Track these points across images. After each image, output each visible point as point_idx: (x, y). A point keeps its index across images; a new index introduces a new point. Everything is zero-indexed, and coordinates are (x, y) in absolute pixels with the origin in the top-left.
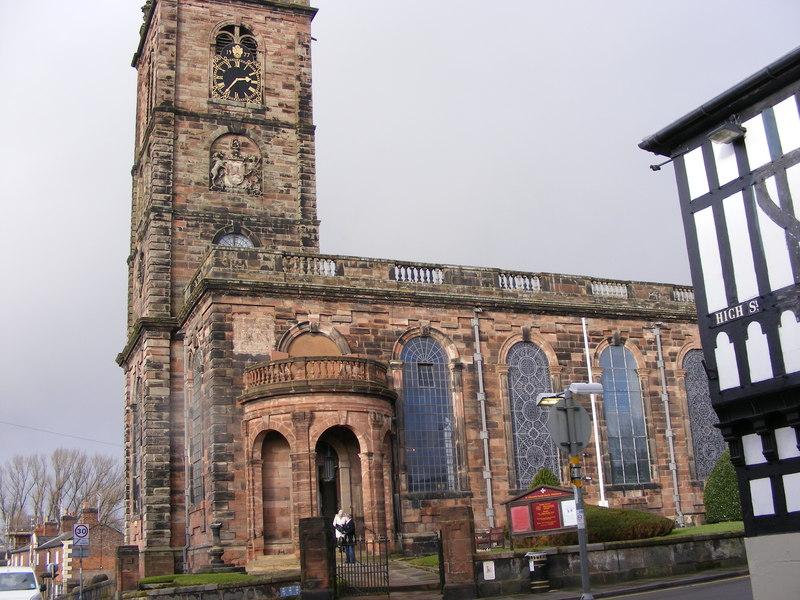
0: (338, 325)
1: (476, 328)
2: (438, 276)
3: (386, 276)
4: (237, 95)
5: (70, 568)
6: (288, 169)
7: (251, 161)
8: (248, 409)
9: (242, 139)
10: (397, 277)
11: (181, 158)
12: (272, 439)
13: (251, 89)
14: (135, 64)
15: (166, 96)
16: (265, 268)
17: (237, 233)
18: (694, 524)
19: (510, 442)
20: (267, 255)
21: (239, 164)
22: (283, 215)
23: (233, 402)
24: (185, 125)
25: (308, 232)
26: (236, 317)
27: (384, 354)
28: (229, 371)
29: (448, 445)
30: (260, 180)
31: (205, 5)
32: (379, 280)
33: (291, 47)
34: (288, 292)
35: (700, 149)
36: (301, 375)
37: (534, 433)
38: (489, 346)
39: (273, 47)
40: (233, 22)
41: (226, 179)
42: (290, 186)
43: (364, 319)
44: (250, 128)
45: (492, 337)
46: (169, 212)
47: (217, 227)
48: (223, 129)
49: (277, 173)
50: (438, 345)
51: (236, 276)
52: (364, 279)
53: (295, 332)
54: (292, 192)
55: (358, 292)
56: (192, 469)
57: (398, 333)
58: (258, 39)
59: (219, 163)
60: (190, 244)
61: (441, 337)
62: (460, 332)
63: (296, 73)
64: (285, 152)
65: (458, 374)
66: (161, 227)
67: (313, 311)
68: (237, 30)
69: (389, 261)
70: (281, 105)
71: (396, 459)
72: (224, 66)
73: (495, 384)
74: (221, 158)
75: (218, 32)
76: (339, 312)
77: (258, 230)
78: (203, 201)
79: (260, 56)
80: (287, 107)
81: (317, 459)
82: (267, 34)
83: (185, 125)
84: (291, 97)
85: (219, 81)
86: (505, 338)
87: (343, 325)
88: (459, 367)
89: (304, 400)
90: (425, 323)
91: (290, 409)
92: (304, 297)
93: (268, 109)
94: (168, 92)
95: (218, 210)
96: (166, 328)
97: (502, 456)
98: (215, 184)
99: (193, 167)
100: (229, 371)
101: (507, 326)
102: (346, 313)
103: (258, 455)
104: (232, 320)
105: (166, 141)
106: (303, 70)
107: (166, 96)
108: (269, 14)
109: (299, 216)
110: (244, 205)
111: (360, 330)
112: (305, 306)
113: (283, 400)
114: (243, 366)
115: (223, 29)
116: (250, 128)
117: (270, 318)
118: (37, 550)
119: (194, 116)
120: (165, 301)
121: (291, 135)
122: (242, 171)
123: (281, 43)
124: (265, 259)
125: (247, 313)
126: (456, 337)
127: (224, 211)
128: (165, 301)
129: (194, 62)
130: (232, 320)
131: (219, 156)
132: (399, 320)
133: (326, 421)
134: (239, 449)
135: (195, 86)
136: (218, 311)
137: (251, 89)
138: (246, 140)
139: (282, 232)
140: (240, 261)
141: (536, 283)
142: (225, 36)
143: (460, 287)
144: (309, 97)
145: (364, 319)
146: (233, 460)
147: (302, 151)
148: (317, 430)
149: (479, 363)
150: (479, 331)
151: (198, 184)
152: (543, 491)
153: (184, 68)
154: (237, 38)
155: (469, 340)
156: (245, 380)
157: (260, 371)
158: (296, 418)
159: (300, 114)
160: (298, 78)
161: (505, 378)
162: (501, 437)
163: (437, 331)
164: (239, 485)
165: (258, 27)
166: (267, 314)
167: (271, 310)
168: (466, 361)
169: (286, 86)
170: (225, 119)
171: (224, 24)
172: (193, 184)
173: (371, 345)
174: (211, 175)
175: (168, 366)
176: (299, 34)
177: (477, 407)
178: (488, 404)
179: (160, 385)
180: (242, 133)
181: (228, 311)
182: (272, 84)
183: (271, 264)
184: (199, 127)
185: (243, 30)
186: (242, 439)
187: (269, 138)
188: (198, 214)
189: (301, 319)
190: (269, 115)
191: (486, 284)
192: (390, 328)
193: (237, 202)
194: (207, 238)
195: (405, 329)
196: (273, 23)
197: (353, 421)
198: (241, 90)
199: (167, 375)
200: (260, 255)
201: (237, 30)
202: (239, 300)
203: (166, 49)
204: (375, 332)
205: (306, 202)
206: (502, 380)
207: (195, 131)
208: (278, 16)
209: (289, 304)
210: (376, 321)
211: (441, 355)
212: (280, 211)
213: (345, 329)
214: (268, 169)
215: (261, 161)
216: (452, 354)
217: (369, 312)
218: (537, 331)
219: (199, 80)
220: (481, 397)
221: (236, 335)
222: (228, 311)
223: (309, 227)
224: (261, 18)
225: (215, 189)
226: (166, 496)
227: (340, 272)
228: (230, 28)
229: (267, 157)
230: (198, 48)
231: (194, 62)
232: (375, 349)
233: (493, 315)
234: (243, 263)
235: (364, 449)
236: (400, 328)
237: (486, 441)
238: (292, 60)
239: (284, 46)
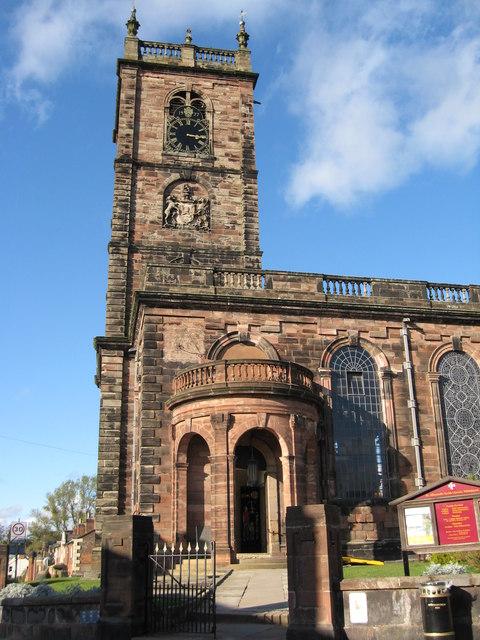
1: (405, 338)
2: (366, 290)
3: (314, 289)
4: (187, 148)
5: (78, 562)
7: (200, 202)
8: (176, 412)
10: (325, 290)
11: (138, 201)
12: (195, 446)
15: (125, 150)
18: (8, 581)
19: (443, 450)
20: (198, 271)
22: (229, 248)
23: (162, 407)
24: (142, 173)
25: (252, 262)
26: (167, 327)
27: (312, 363)
28: (159, 378)
30: (208, 219)
31: (161, 76)
32: (309, 290)
33: (236, 106)
36: (220, 378)
37: (467, 441)
38: (419, 355)
39: (219, 108)
40: (184, 89)
41: (178, 218)
42: (235, 223)
44: (199, 175)
45: (421, 346)
49: (223, 212)
50: (367, 354)
52: (293, 292)
54: (237, 228)
57: (326, 342)
58: (207, 101)
59: (171, 204)
61: (369, 346)
62: (389, 342)
63: (240, 128)
64: (231, 194)
65: (387, 382)
66: (118, 259)
67: (242, 322)
68: (188, 95)
69: (316, 275)
70: (227, 155)
71: (324, 465)
72: (177, 125)
73: (425, 391)
74: (174, 201)
76: (267, 322)
77: (206, 261)
78: (156, 237)
79: (209, 117)
81: (236, 465)
82: (214, 98)
84: (236, 148)
85: (172, 137)
86: (434, 347)
87: (272, 334)
88: (388, 375)
89: (224, 402)
90: (354, 333)
91: (210, 411)
92: (232, 309)
93: (215, 159)
94: (127, 147)
95: (171, 244)
96: (119, 348)
97: (435, 463)
98: (168, 221)
99: (150, 207)
100: (159, 378)
101: (437, 336)
102: (273, 323)
103: (183, 459)
104: (163, 330)
105: (124, 187)
107: (125, 150)
108: (216, 81)
109: (243, 248)
110: (193, 240)
112: (235, 317)
113: (204, 403)
114: (173, 374)
116: (199, 175)
118: (64, 545)
119: (150, 166)
120: (120, 323)
121: (237, 180)
122: (192, 211)
124: (196, 274)
125: (178, 324)
126: (385, 346)
127: (176, 247)
128: (120, 323)
129: (151, 122)
130: (163, 330)
131: (171, 199)
132: (327, 329)
133: (243, 424)
134: (166, 453)
135: (151, 142)
136: (150, 322)
140: (172, 276)
141: (464, 296)
143: (386, 299)
144: (252, 147)
146: (160, 464)
147: (246, 193)
148: (236, 432)
149: (409, 372)
150: (409, 341)
151: (152, 222)
152: (451, 486)
154: (188, 102)
155: (398, 350)
156: (174, 386)
157: (186, 376)
158: (214, 419)
160: (242, 132)
161: (435, 385)
162: (433, 444)
163: (365, 340)
164: (165, 487)
165: (206, 92)
167: (201, 321)
168: (395, 370)
169: (231, 139)
170: (177, 167)
172: (148, 222)
173: (299, 353)
174: (164, 215)
175: (121, 381)
176: (242, 96)
177: (407, 414)
178: (417, 411)
179: (113, 398)
182: (219, 138)
183: (202, 279)
184: (155, 175)
185: (194, 95)
186: (170, 443)
187: (216, 183)
188: (151, 248)
189: (230, 329)
190: (217, 164)
191: (414, 296)
192: (318, 338)
193: (187, 237)
195: (334, 339)
196: (219, 88)
197: (274, 423)
198: (190, 145)
199: (120, 389)
200: (192, 271)
201: (188, 95)
202: (170, 312)
203: (126, 112)
204: (303, 341)
206: (433, 388)
207: (151, 178)
208: (224, 82)
209: (218, 315)
210: (304, 331)
211: (371, 364)
213: (274, 338)
214: (215, 209)
215: (209, 202)
216: (381, 362)
217: (298, 323)
218: (466, 340)
219: (154, 137)
220: (411, 404)
221: (167, 344)
223: (252, 257)
225: (168, 227)
226: (115, 499)
227: (269, 285)
228: (183, 94)
230: (154, 111)
231: (151, 122)
232: (304, 354)
233: (421, 325)
234: (176, 278)
235: (285, 452)
236: (328, 338)
237: (417, 449)
238: (236, 117)
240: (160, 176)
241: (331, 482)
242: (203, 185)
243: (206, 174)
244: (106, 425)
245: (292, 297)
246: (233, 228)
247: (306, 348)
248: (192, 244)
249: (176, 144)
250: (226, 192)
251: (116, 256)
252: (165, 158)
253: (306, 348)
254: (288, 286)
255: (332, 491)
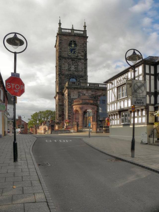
0: (88, 94)
3: (98, 86)
6: (82, 67)
9: (74, 62)
13: (76, 53)
14: (55, 47)
16: (76, 85)
17: (73, 78)
21: (73, 66)
22: (81, 75)
27: (96, 99)
29: (10, 94)
34: (80, 88)
35: (130, 72)
39: (79, 44)
40: (72, 40)
42: (82, 70)
43: (93, 93)
44: (75, 60)
46: (61, 75)
47: (70, 77)
48: (70, 60)
51: (71, 86)
52: (94, 87)
53: (81, 95)
55: (92, 89)
56: (108, 136)
57: (99, 95)
58: (77, 43)
59: (70, 66)
60: (65, 80)
64: (82, 64)
67: (85, 92)
68: (73, 42)
72: (71, 49)
75: (69, 42)
78: (67, 73)
80: (82, 56)
83: (64, 60)
84: (83, 54)
85: (70, 51)
87: (90, 94)
90: (104, 94)
98: (69, 70)
99: (65, 67)
106: (85, 48)
111: (93, 95)
112: (83, 91)
114: (72, 100)
115: (70, 41)
117: (77, 93)
119: (65, 58)
120: (61, 89)
121: (83, 61)
122: (74, 67)
123: (81, 43)
125: (73, 92)
127: (71, 74)
128: (61, 89)
130: (71, 93)
135: (65, 53)
137: (76, 53)
138: (75, 62)
139: (81, 78)
142: (71, 43)
145: (93, 93)
151: (66, 70)
153: (63, 49)
159: (85, 57)
160: (84, 50)
165: (77, 41)
166: (77, 92)
167: (77, 91)
170: (71, 58)
171: (70, 41)
179: (60, 102)
180: (74, 61)
181: (70, 92)
183: (77, 84)
184: (66, 60)
185: (74, 42)
187: (79, 61)
189: (82, 93)
190: (79, 57)
192: (98, 94)
194: (68, 79)
196: (80, 40)
201: (73, 42)
202: (72, 90)
205: (86, 72)
207: (65, 61)
208: (81, 38)
209: (80, 90)
212: (81, 74)
213: (90, 94)
214: (79, 67)
219: (66, 51)
221: (71, 95)
222: (70, 92)
224: (77, 39)
225: (69, 71)
228: (72, 41)
229: (78, 65)
239: (82, 44)
240: (67, 60)
241: (98, 117)
242: (76, 62)
243: (77, 60)
244: (59, 107)
245: (93, 88)
246: (82, 71)
247: (95, 96)
248: (74, 74)
249: (70, 53)
250: (81, 63)
251: (59, 77)
252: (68, 56)
253: (95, 96)
254: (93, 86)
255: (98, 118)
